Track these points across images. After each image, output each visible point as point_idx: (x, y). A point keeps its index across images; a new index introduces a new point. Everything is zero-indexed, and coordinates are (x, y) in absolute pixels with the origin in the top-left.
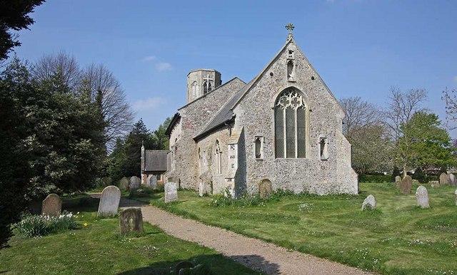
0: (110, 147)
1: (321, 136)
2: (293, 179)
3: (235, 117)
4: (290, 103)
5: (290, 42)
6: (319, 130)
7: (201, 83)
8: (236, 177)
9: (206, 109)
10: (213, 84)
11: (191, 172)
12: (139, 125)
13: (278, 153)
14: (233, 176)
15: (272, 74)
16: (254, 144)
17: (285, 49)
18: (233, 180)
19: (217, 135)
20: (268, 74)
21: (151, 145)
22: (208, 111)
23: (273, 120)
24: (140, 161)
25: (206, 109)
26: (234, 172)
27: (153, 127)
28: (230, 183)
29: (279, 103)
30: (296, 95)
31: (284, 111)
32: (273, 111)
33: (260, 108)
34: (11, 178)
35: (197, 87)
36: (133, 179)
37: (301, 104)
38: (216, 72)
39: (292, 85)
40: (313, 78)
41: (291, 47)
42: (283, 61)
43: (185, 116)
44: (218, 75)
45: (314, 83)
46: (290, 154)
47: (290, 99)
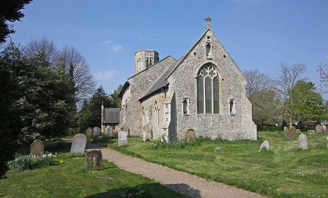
0: (79, 106)
1: (230, 98)
2: (210, 129)
3: (168, 84)
4: (208, 74)
5: (208, 30)
6: (229, 93)
7: (145, 60)
8: (169, 128)
9: (148, 78)
10: (153, 61)
11: (137, 124)
12: (100, 90)
13: (200, 110)
14: (167, 127)
15: (195, 54)
16: (183, 104)
17: (204, 35)
18: (167, 130)
19: (156, 97)
20: (192, 53)
21: (108, 105)
22: (150, 80)
23: (196, 87)
24: (100, 116)
25: (148, 78)
26: (168, 124)
27: (110, 91)
28: (165, 132)
29: (201, 74)
30: (213, 68)
31: (204, 80)
32: (196, 80)
33: (187, 78)
34: (8, 128)
35: (142, 62)
36: (96, 129)
37: (216, 75)
38: (155, 52)
39: (210, 61)
40: (225, 56)
41: (209, 34)
42: (203, 44)
43: (133, 83)
44: (156, 54)
45: (225, 59)
46: (208, 111)
47: (208, 71)
